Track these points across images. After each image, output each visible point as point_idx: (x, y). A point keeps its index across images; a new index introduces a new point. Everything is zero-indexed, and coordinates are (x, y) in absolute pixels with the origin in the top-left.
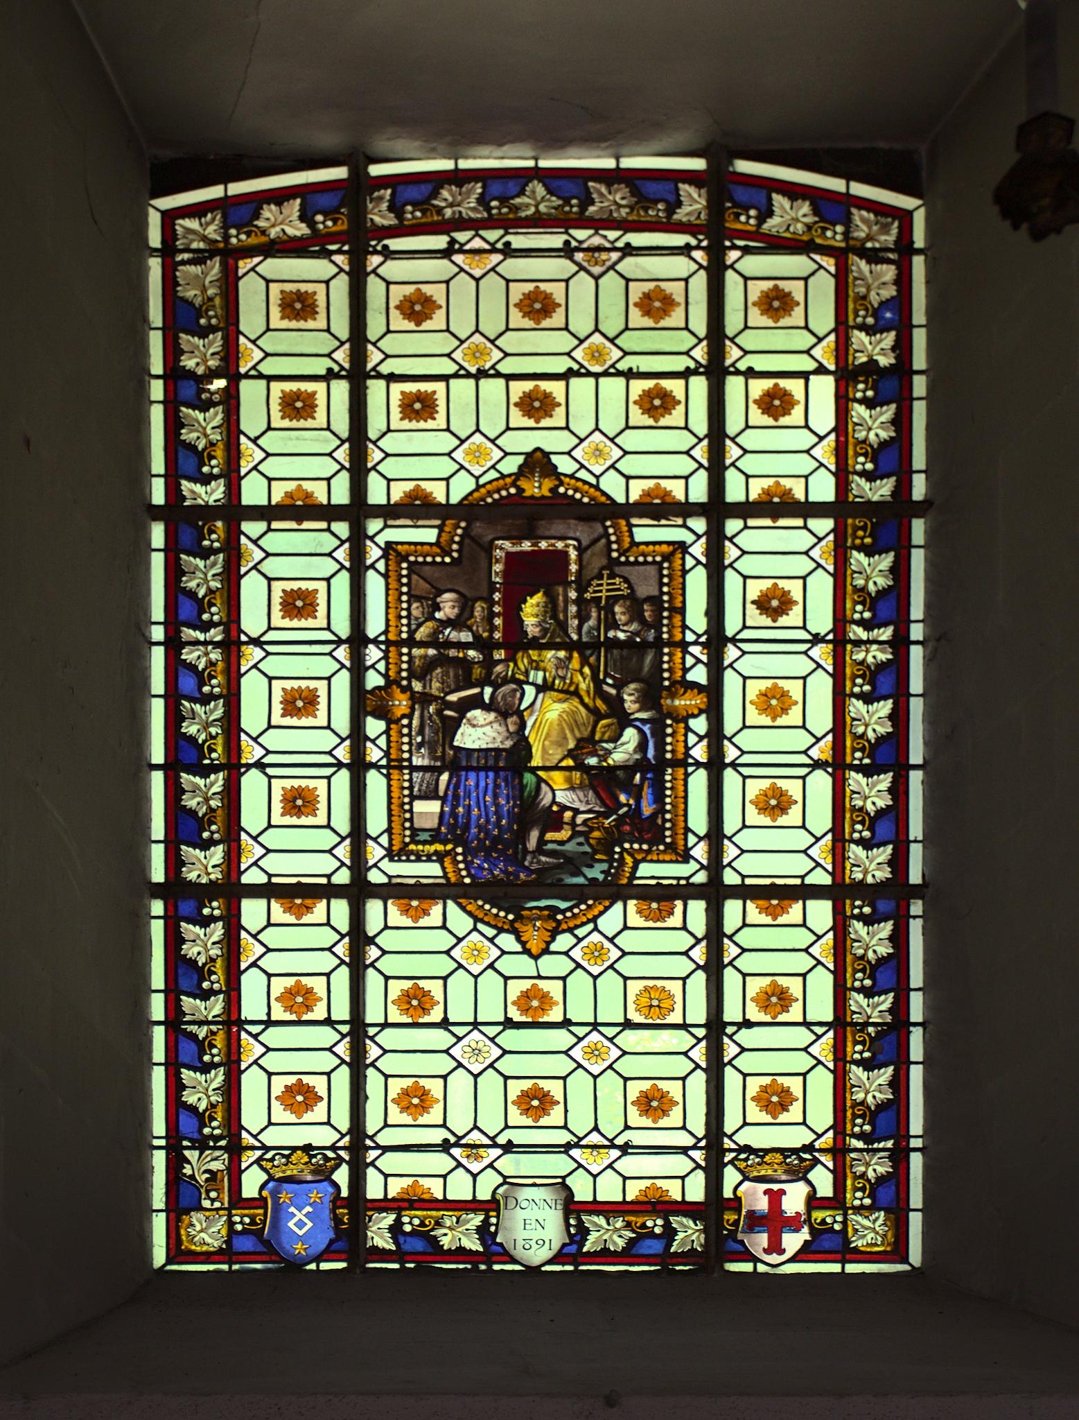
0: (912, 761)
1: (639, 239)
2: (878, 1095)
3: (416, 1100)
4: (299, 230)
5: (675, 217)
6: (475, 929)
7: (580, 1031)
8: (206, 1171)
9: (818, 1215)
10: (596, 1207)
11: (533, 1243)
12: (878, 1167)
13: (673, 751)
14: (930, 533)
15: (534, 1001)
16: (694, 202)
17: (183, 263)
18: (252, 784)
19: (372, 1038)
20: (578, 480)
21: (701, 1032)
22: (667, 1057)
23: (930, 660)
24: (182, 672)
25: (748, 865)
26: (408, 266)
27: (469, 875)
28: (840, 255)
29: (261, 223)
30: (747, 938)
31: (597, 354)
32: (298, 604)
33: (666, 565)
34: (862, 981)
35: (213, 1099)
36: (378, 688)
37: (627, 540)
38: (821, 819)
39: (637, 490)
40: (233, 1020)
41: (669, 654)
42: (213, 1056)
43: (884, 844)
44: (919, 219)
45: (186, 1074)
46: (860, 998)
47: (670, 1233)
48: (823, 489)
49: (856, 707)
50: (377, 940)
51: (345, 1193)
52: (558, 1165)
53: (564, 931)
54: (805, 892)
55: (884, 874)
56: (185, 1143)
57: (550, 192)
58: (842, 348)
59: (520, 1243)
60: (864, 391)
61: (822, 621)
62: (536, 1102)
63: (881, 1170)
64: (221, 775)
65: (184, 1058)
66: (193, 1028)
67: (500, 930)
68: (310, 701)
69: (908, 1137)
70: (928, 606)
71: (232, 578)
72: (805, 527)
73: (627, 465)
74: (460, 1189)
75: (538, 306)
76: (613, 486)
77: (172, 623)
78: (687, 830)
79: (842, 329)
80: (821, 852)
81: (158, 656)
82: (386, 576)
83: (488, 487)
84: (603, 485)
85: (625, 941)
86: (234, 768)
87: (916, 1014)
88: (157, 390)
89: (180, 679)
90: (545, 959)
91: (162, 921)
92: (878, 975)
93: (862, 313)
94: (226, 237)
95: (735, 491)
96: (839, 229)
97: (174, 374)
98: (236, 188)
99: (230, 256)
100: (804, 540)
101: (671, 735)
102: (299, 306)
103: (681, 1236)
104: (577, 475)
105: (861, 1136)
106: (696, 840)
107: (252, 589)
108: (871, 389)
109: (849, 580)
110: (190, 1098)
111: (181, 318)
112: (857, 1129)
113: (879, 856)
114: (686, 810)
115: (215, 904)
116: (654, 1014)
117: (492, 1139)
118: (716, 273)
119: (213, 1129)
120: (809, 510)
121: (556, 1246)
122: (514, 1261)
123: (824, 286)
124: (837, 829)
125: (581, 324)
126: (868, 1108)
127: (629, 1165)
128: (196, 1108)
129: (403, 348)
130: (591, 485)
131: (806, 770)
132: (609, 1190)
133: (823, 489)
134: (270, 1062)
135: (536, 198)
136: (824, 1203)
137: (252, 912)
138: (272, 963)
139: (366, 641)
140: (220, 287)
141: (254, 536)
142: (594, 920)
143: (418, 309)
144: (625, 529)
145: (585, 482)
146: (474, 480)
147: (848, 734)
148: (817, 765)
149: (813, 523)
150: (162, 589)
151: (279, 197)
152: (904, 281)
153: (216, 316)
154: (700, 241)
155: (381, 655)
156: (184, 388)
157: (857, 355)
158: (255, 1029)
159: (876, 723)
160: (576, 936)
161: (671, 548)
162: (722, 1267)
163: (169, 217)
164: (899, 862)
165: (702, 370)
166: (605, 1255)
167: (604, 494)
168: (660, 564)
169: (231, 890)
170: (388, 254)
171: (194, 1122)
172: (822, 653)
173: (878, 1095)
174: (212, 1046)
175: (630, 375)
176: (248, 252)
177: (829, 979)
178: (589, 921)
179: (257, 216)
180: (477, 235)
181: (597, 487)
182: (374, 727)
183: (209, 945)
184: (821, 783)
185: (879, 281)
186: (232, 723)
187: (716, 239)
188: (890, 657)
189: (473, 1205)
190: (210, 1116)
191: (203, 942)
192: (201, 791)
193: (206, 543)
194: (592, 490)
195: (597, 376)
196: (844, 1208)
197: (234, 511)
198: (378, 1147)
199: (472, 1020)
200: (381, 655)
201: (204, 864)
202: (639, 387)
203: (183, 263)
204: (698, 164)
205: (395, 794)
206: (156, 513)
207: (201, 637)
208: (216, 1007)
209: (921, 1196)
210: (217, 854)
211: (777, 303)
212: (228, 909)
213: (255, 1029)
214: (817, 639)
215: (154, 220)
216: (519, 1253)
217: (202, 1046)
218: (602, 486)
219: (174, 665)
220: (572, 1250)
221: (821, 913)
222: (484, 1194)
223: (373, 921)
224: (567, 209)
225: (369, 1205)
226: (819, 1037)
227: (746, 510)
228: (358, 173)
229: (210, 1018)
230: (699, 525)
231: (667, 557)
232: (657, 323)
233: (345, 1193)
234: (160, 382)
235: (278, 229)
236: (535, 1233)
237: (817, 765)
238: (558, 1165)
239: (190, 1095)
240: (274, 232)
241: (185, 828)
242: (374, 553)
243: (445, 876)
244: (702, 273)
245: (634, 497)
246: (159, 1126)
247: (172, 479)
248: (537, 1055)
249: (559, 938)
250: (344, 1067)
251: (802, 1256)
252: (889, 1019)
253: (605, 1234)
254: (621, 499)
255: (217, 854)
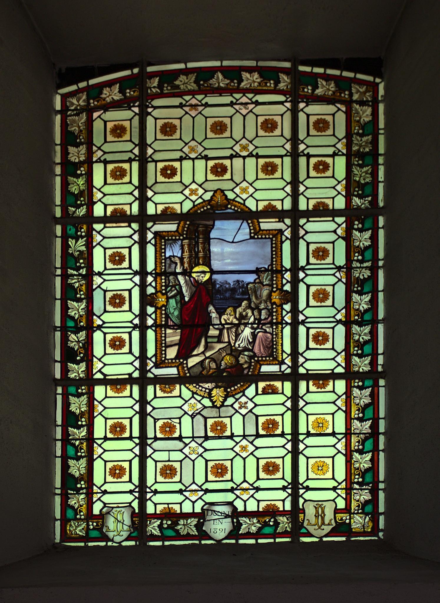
0: (380, 152)
1: (261, 98)
2: (364, 337)
3: (168, 471)
4: (117, 97)
5: (278, 88)
6: (193, 397)
7: (237, 439)
8: (78, 251)
9: (339, 516)
10: (246, 514)
11: (218, 530)
12: (365, 496)
13: (276, 319)
14: (386, 221)
15: (219, 170)
16: (285, 81)
17: (70, 115)
18: (98, 336)
19: (150, 445)
20: (236, 201)
21: (289, 437)
22: (275, 448)
23: (387, 244)
24: (69, 258)
25: (309, 365)
26: (164, 110)
27: (189, 372)
28: (348, 103)
29: (103, 96)
30: (309, 398)
31: (244, 148)
32: (117, 259)
33: (274, 239)
34: (358, 383)
35: (81, 313)
36: (152, 294)
37: (258, 228)
38: (340, 345)
39: (261, 206)
40: (90, 439)
41: (276, 277)
42: (81, 516)
43: (368, 230)
44: (381, 87)
45: (71, 179)
46: (357, 359)
47: (276, 524)
48: (340, 203)
49: (355, 297)
50: (152, 199)
51: (137, 511)
52: (230, 497)
53: (230, 396)
54: (333, 376)
55: (367, 369)
56: (69, 492)
57: (225, 77)
58: (349, 145)
59: (212, 530)
60: (358, 479)
61: (341, 261)
62: (220, 470)
63: (367, 498)
64: (85, 146)
65: (69, 265)
66: (73, 442)
67: (203, 397)
68: (123, 428)
69: (379, 129)
70: (386, 124)
71: (90, 247)
72: (333, 220)
73: (257, 195)
74: (187, 508)
75: (219, 128)
76: (251, 204)
77: (64, 267)
78: (283, 351)
79: (349, 136)
80: (340, 359)
81: (58, 281)
82: (155, 245)
83: (198, 206)
84: (247, 204)
85: (257, 400)
86: (90, 329)
87: (382, 429)
88: (58, 170)
89: (67, 197)
90: (222, 409)
91: (60, 459)
92: (366, 412)
93: (357, 128)
94: (89, 104)
95: (302, 205)
96: (347, 93)
97: (65, 163)
98: (92, 82)
99: (90, 111)
100: (333, 226)
101: (276, 312)
102: (119, 131)
103: (281, 525)
104: (236, 199)
105: (358, 483)
106: (287, 356)
107: (98, 254)
108: (360, 287)
109: (353, 496)
110: (72, 313)
111: (69, 139)
112: (356, 258)
113: (365, 298)
114: (281, 254)
115: (83, 388)
116: (270, 428)
117: (200, 487)
118: (295, 112)
119: (82, 453)
120: (334, 213)
121: (227, 532)
122: (211, 538)
123: (341, 118)
124: (347, 349)
125: (237, 135)
126: (361, 248)
127: (260, 495)
128: (74, 507)
129: (162, 148)
130: (241, 204)
131: (334, 324)
132: (252, 506)
133: (340, 203)
134: (106, 243)
135: (220, 80)
136: (341, 511)
137: (99, 391)
138: (106, 243)
139: (148, 274)
140: (85, 125)
141: (98, 230)
142: (243, 392)
143: (168, 130)
144: (257, 224)
145: (239, 203)
146: (192, 203)
147: (352, 309)
148: (339, 322)
149: (337, 219)
150: (60, 128)
151: (110, 84)
152: (375, 114)
153: (83, 138)
154: (287, 98)
155: (153, 279)
156: (70, 169)
157: (355, 335)
158: (99, 442)
159: (364, 463)
160: (235, 398)
161: (277, 232)
162: (299, 540)
163: (64, 97)
164: (373, 363)
165: (288, 154)
166: (248, 535)
167: (247, 207)
168: (272, 239)
169: (90, 382)
170: (155, 108)
171: (73, 261)
172: (341, 275)
173: (364, 337)
174: (81, 449)
175: (258, 156)
176: (96, 109)
177: (343, 116)
178: (241, 392)
179: (101, 93)
180: (193, 97)
181: (244, 204)
182: (150, 310)
183: (80, 372)
184: (341, 329)
185: (365, 114)
186: (90, 312)
187: (295, 96)
188: (370, 338)
189: (193, 515)
190: (80, 510)
191: (78, 405)
192: (75, 340)
193: (78, 296)
194: (242, 206)
195: (244, 158)
196: (350, 513)
197: (90, 219)
198: (152, 107)
199: (191, 436)
200: (153, 279)
201: (77, 371)
202: (261, 161)
203: (70, 115)
204: (287, 65)
205: (158, 337)
206: (57, 221)
207: (75, 273)
208: (83, 432)
209: (383, 341)
210: (83, 366)
211: (321, 125)
212: (89, 389)
213: (99, 442)
214: (339, 268)
215: (58, 100)
216: (212, 535)
217: (77, 449)
218: (246, 204)
219: (65, 505)
220: (235, 533)
221: (341, 386)
222: (198, 510)
223: (150, 395)
224: (232, 84)
225: (148, 516)
226: (339, 440)
227: (308, 214)
228: (142, 70)
229: (81, 437)
230: (288, 221)
231: (275, 236)
232: (270, 203)
233: (137, 511)
234: (59, 166)
235: (110, 97)
236: (219, 528)
237: (339, 322)
238: (230, 497)
239: (71, 374)
240: (108, 100)
241: (69, 355)
242: (150, 236)
243: (179, 374)
244: (289, 197)
245: (260, 208)
246: (58, 483)
247: (64, 207)
248: (219, 450)
249: (229, 399)
250: (137, 287)
251: (332, 534)
252: (370, 431)
253: (249, 525)
254: (254, 209)
255: (83, 366)
